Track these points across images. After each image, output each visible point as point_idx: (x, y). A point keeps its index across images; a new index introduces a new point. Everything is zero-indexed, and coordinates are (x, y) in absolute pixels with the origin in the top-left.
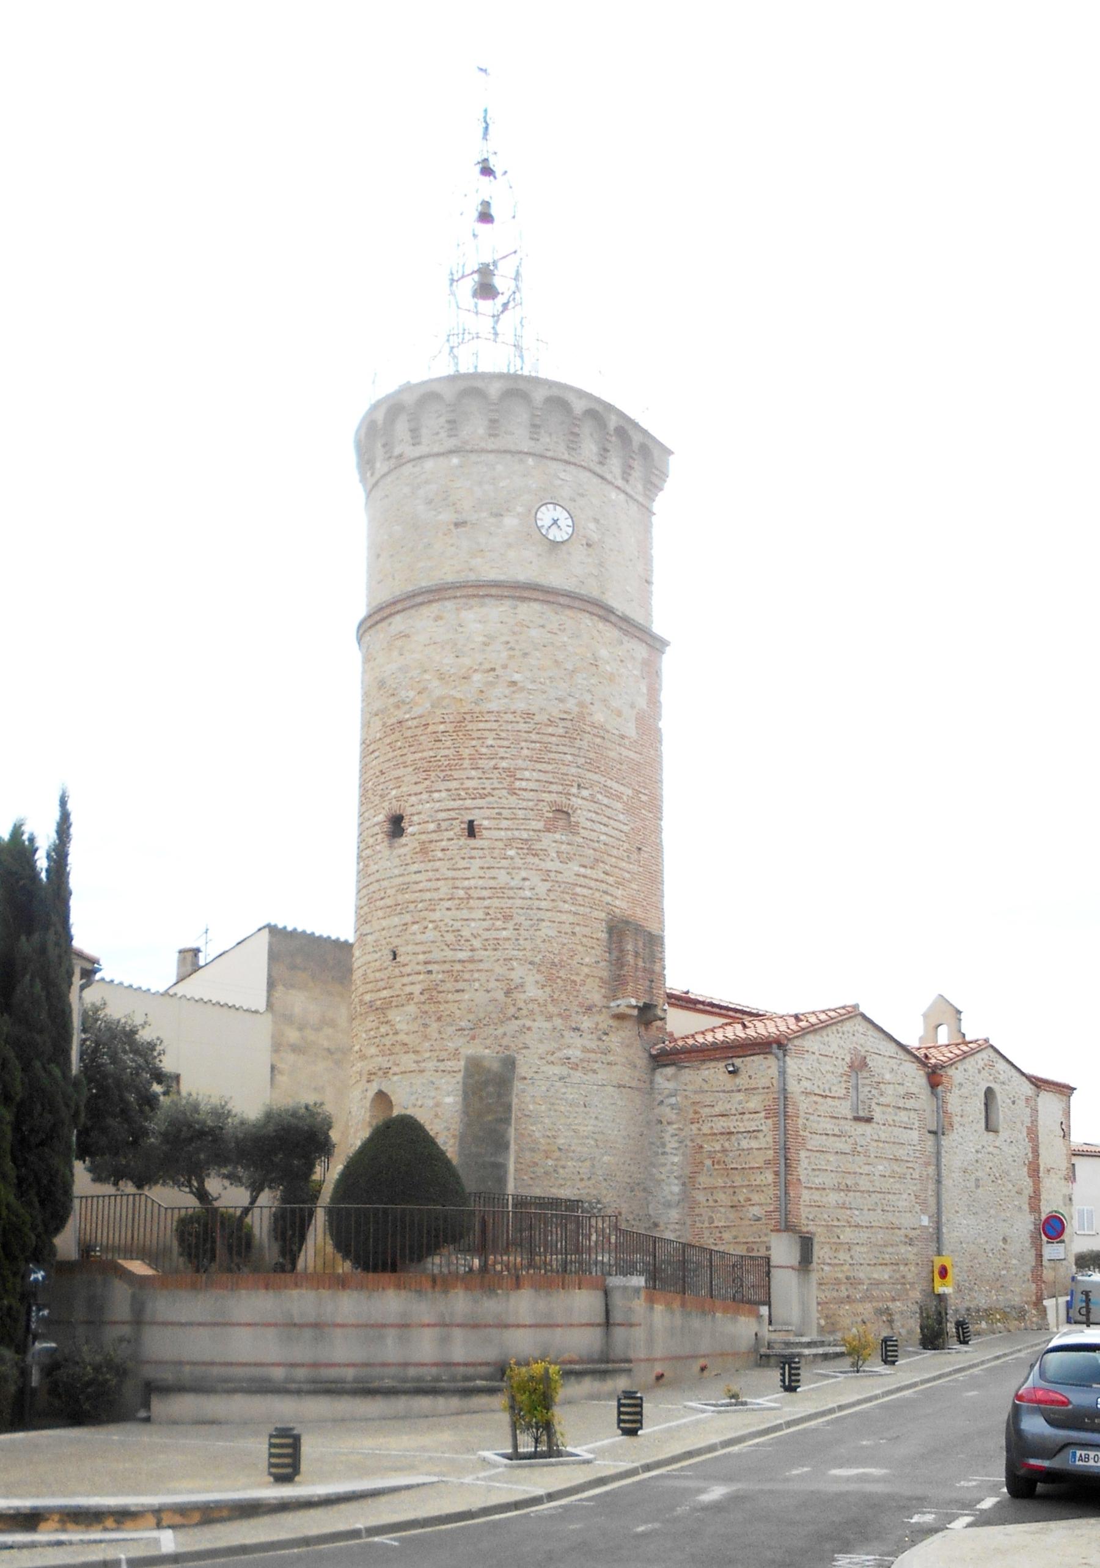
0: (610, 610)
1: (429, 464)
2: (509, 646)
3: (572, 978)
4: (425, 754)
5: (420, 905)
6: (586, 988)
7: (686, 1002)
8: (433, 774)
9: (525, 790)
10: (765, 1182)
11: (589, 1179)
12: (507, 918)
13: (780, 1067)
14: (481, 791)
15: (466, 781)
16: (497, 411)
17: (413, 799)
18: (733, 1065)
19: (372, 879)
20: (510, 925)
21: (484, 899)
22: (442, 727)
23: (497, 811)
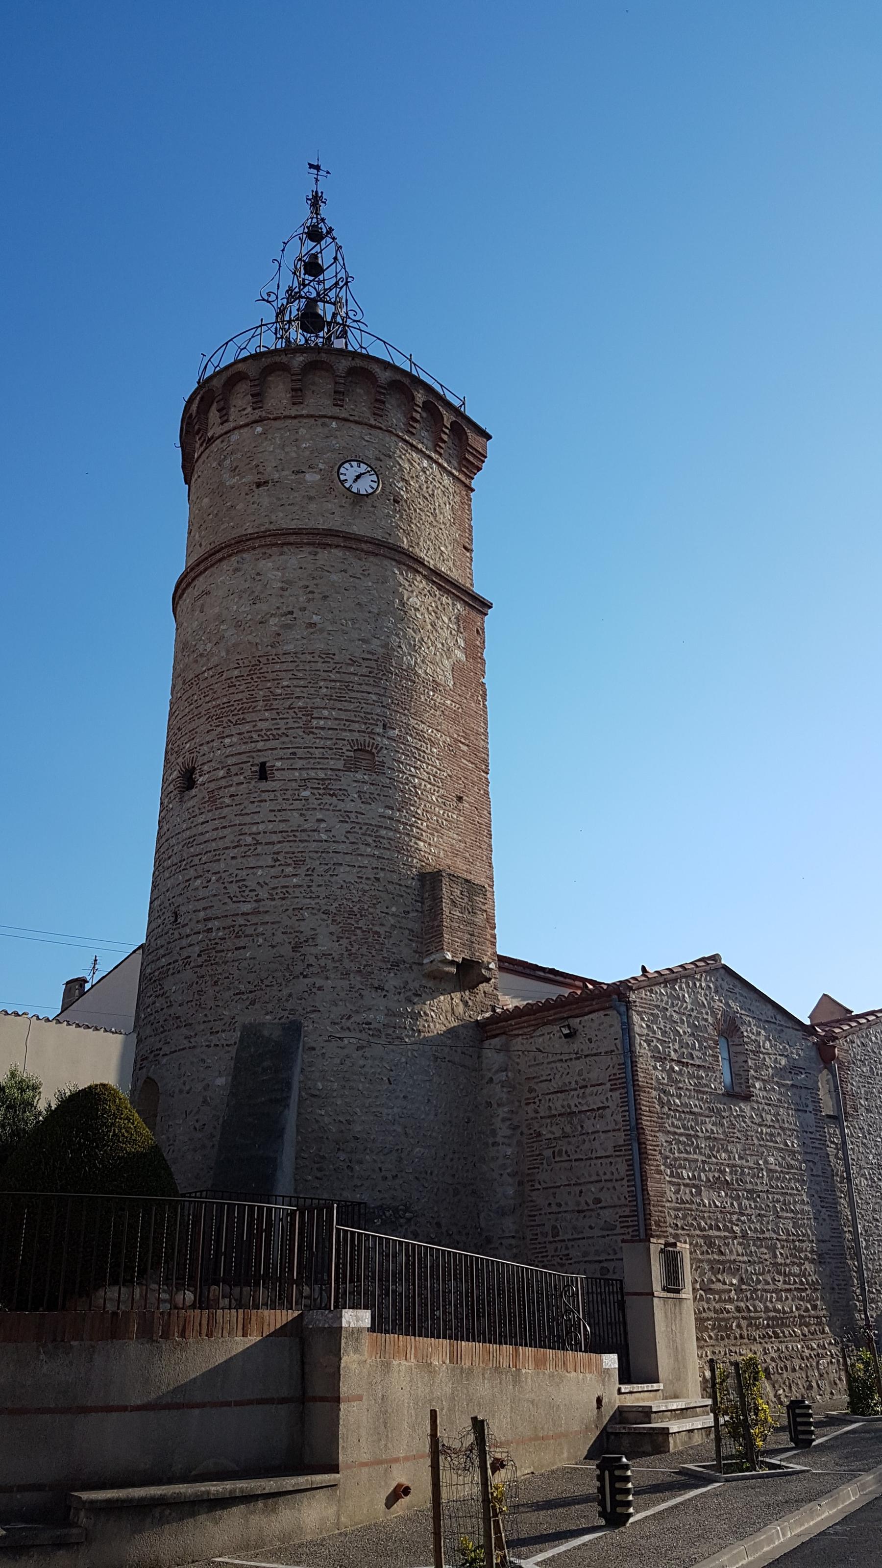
0: (421, 563)
1: (235, 437)
2: (308, 590)
7: (510, 965)
8: (225, 720)
9: (323, 728)
10: (616, 1176)
12: (297, 864)
13: (623, 1024)
14: (275, 732)
15: (259, 724)
20: (302, 871)
21: (273, 843)
22: (236, 673)
23: (291, 751)
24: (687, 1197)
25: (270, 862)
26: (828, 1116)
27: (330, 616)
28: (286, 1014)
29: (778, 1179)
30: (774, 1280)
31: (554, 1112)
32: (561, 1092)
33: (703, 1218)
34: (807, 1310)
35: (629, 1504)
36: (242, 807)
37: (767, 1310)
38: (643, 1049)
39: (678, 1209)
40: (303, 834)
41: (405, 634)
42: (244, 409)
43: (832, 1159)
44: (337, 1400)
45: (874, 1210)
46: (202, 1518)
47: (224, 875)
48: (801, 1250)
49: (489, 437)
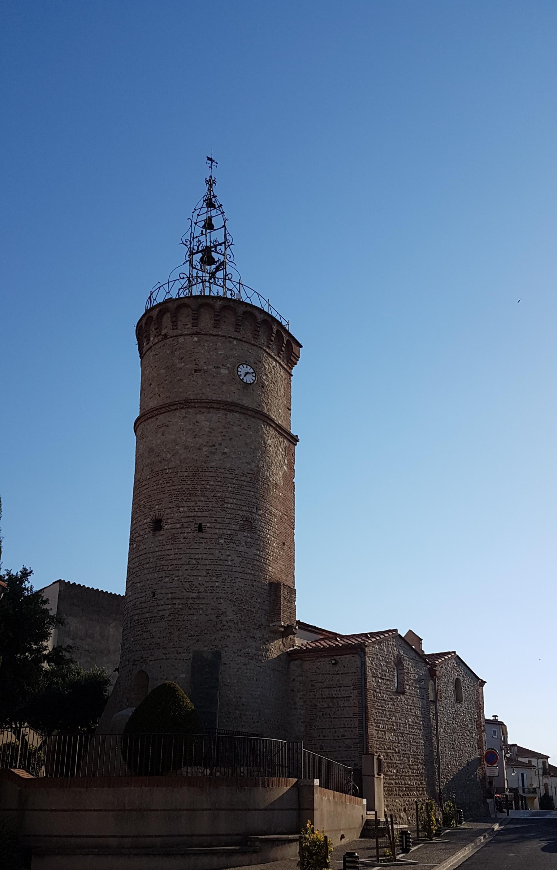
0: (272, 420)
1: (181, 339)
2: (223, 434)
3: (252, 609)
4: (176, 487)
5: (170, 568)
6: (258, 615)
7: (304, 627)
11: (258, 722)
12: (218, 576)
14: (206, 508)
15: (198, 503)
16: (219, 316)
17: (168, 511)
18: (335, 660)
19: (142, 552)
20: (220, 580)
22: (186, 474)
23: (215, 519)
24: (381, 736)
25: (205, 574)
26: (431, 701)
27: (233, 449)
28: (214, 647)
29: (412, 728)
30: (408, 771)
31: (324, 696)
32: (328, 688)
33: (386, 744)
34: (419, 785)
35: (410, 846)
36: (190, 544)
37: (405, 784)
38: (369, 673)
39: (377, 741)
40: (221, 561)
41: (266, 460)
42: (187, 325)
43: (431, 719)
44: (313, 810)
45: (445, 743)
46: (287, 845)
47: (181, 578)
48: (418, 759)
49: (301, 347)
